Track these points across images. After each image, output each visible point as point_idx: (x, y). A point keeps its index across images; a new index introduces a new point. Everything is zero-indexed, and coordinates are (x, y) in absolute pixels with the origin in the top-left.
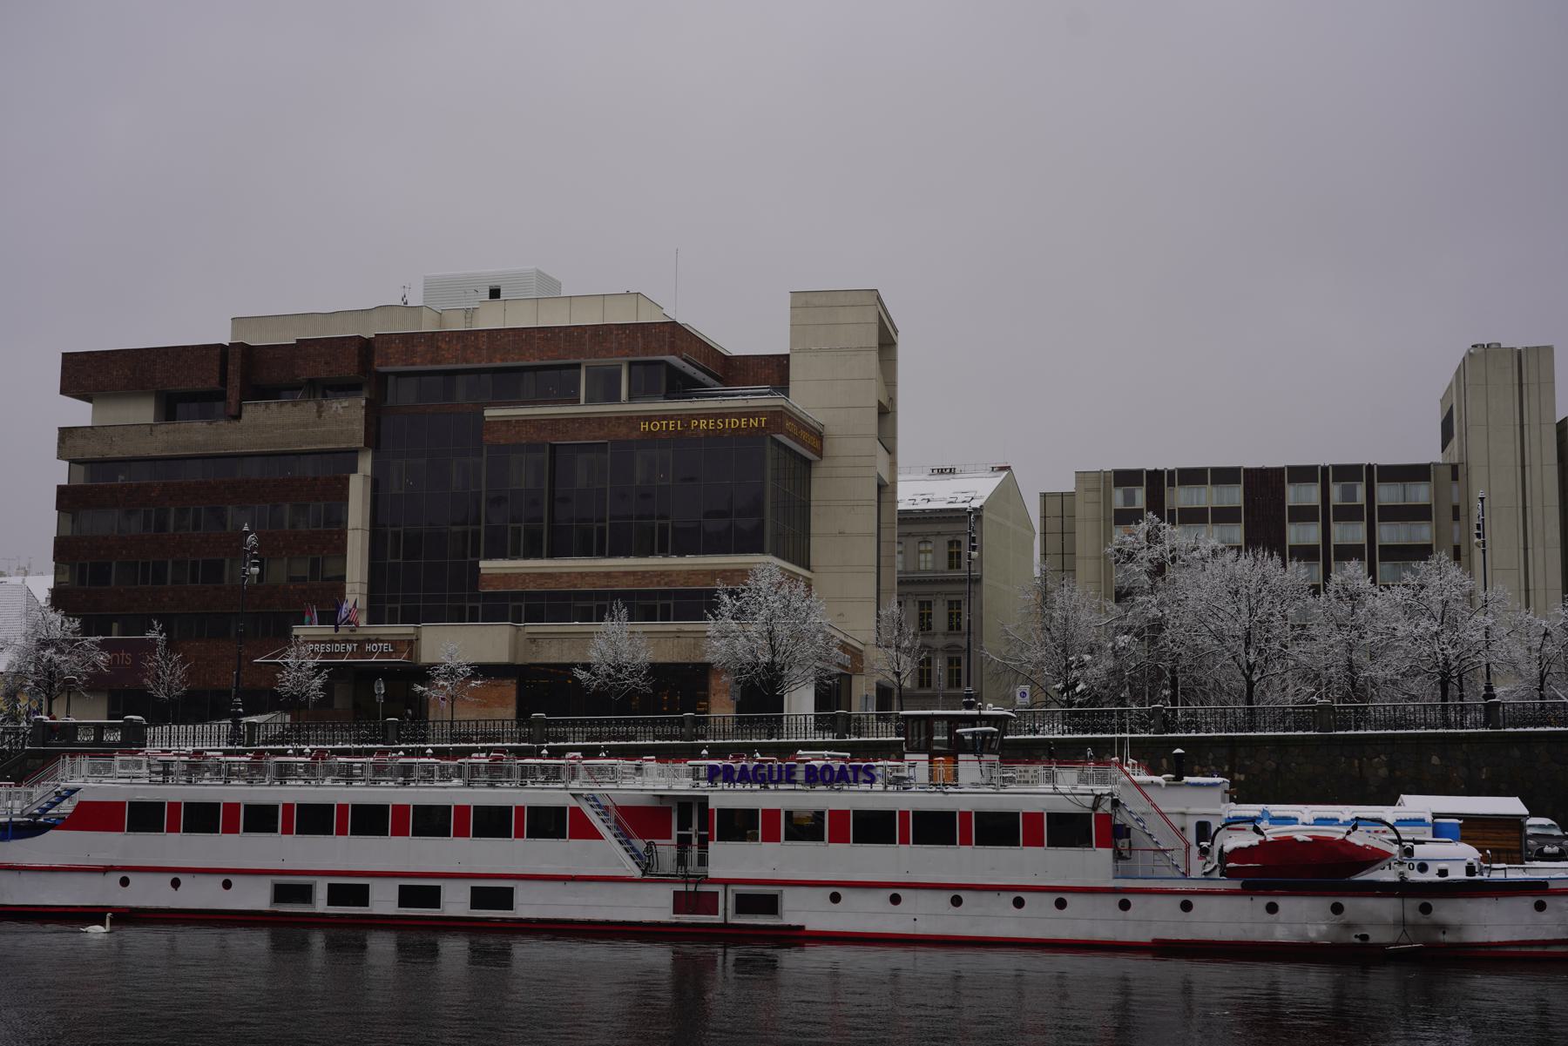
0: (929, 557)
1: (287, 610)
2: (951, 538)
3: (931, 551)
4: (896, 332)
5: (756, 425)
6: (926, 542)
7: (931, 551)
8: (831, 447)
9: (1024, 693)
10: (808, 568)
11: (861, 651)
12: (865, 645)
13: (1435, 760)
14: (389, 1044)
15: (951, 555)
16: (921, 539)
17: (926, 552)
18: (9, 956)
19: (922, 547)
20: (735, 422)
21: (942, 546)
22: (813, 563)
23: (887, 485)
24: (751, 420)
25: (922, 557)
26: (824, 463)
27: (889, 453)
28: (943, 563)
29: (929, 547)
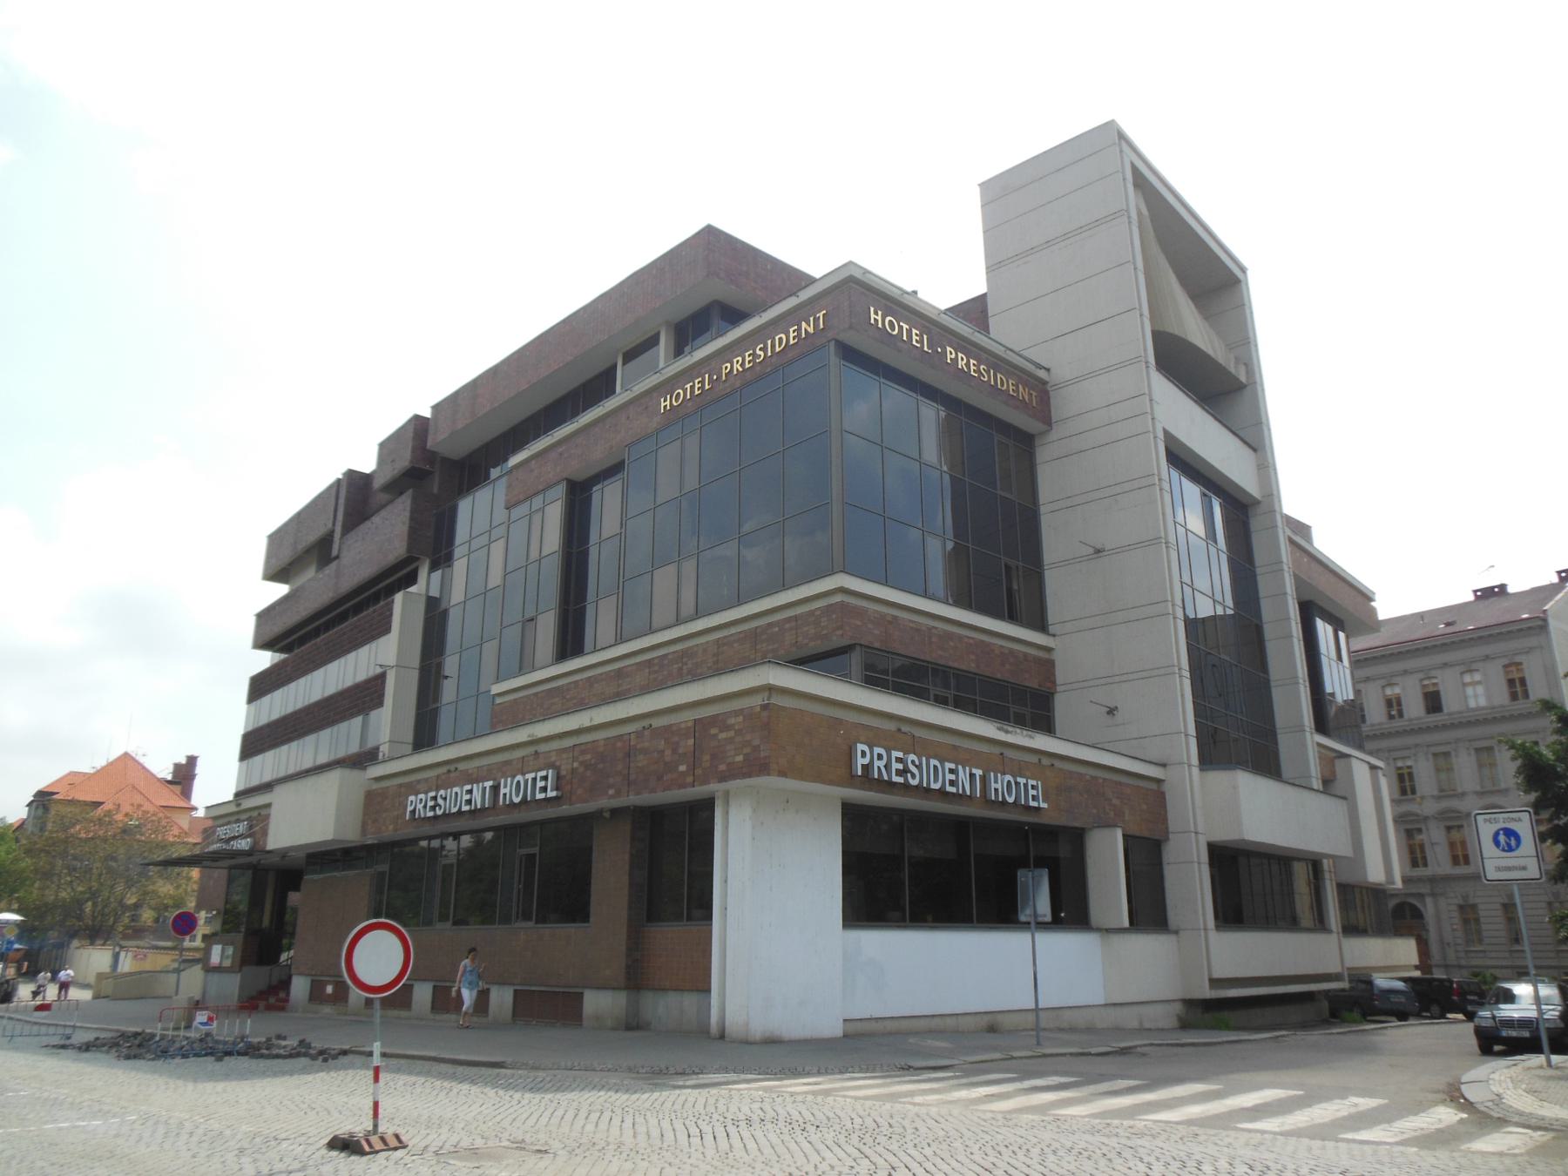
0: (1480, 689)
1: (905, 829)
2: (1505, 661)
3: (1479, 683)
4: (1243, 270)
5: (811, 330)
6: (1470, 671)
7: (1479, 683)
8: (1061, 406)
9: (1509, 833)
10: (1041, 625)
11: (1159, 781)
12: (1164, 765)
13: (1063, 915)
14: (1373, 1174)
15: (1511, 682)
16: (1463, 668)
17: (1474, 684)
18: (445, 1142)
19: (1467, 679)
20: (780, 339)
21: (1495, 674)
22: (1053, 615)
23: (1258, 502)
24: (804, 324)
25: (1470, 691)
26: (1054, 435)
27: (1255, 450)
28: (1502, 696)
29: (1477, 677)
